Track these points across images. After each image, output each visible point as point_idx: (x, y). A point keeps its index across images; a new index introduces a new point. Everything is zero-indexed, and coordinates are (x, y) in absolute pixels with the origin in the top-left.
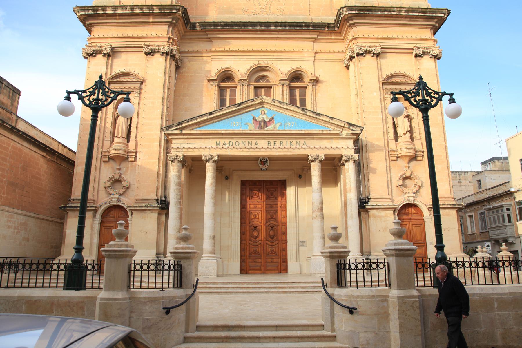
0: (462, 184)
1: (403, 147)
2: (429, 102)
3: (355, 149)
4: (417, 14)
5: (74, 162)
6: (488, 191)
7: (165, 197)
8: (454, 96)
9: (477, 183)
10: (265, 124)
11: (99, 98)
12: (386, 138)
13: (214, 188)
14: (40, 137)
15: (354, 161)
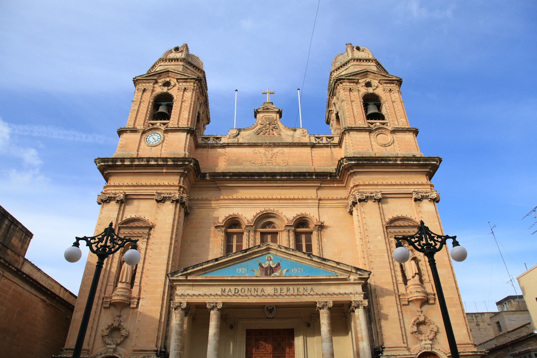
0: (480, 327)
1: (413, 290)
2: (433, 246)
3: (364, 294)
4: (412, 162)
5: (74, 307)
6: (510, 334)
7: (165, 348)
8: (457, 239)
9: (496, 325)
10: (272, 270)
11: (109, 243)
12: (395, 281)
13: (217, 338)
14: (43, 280)
15: (364, 307)
